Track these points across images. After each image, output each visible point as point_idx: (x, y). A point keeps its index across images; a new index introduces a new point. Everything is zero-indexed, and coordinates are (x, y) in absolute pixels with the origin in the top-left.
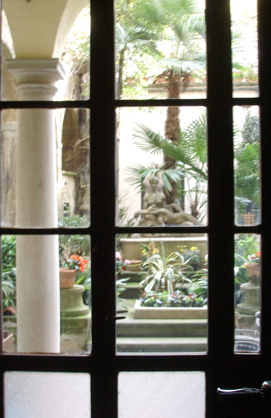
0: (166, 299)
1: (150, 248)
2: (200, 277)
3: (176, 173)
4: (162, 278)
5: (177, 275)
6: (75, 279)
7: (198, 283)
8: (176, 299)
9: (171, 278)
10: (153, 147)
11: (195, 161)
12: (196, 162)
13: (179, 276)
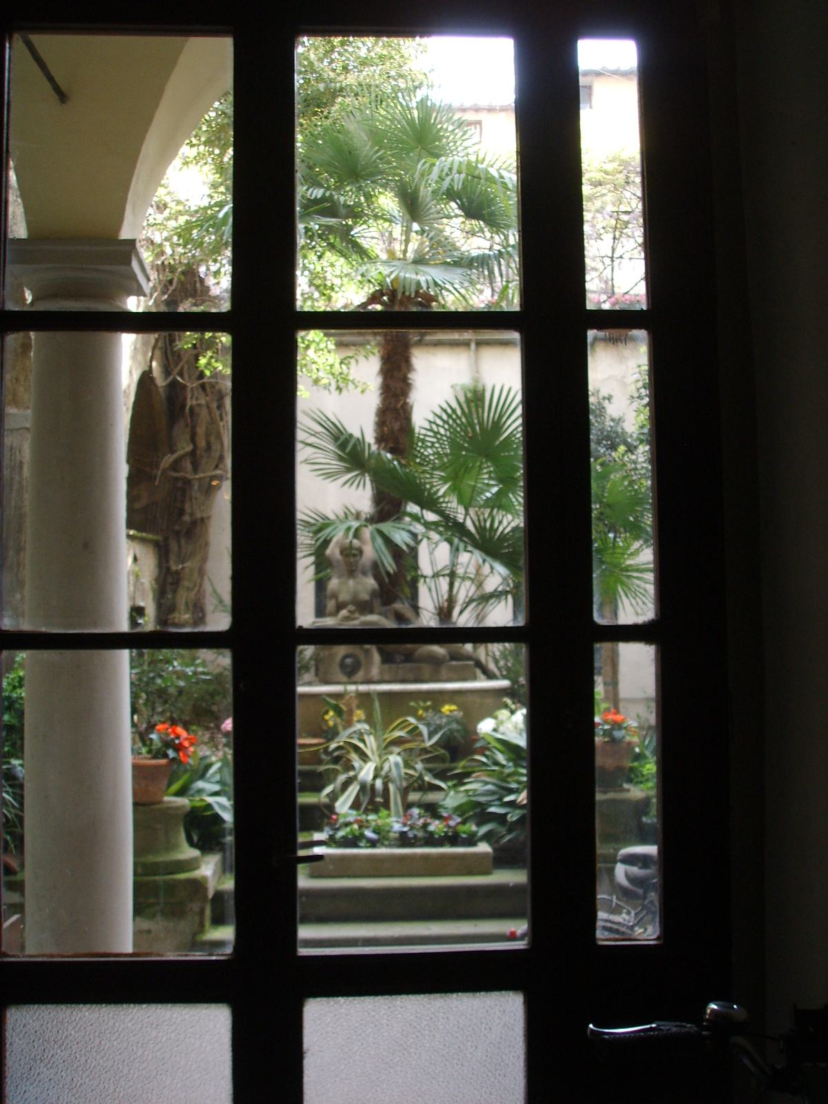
0: (387, 829)
1: (344, 708)
2: (468, 775)
3: (403, 529)
4: (375, 777)
5: (411, 772)
6: (165, 782)
7: (463, 788)
8: (410, 830)
9: (397, 779)
10: (348, 470)
11: (447, 503)
12: (449, 505)
13: (417, 775)
